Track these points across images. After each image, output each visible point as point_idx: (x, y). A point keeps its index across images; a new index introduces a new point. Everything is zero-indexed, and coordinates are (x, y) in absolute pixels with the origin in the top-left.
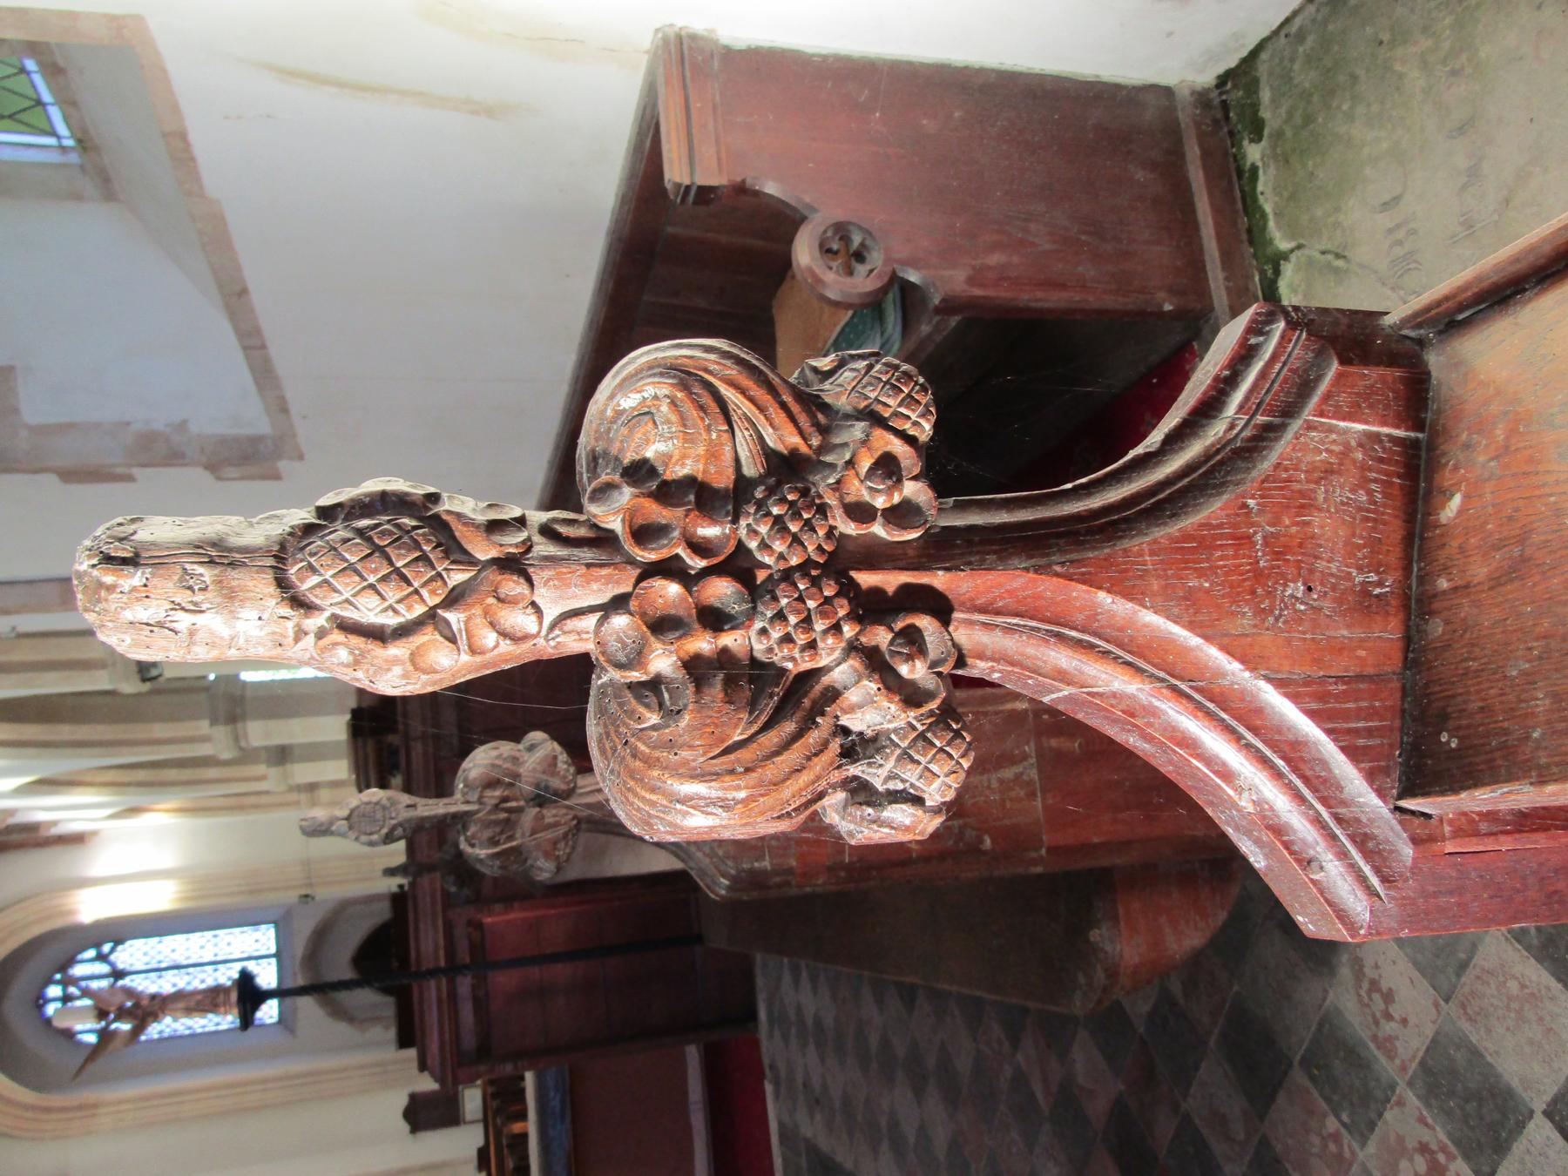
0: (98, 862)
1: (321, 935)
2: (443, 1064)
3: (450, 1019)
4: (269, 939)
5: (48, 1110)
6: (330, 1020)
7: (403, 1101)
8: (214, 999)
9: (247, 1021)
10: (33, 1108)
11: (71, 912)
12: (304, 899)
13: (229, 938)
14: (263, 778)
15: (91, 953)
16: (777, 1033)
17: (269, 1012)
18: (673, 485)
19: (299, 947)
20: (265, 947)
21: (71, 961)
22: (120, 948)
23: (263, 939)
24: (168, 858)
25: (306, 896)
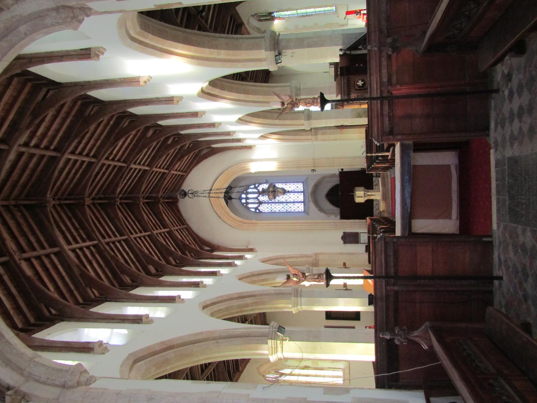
0: (255, 154)
1: (317, 186)
2: (378, 136)
3: (381, 121)
4: (301, 187)
5: (244, 223)
6: (319, 212)
7: (342, 234)
8: (313, 100)
9: (322, 108)
10: (240, 222)
11: (249, 169)
12: (313, 171)
13: (290, 186)
14: (303, 125)
15: (253, 186)
16: (499, 127)
17: (328, 107)
18: (394, 227)
19: (310, 189)
20: (300, 189)
21: (248, 188)
22: (260, 186)
23: (299, 187)
24: (275, 154)
25: (314, 170)
